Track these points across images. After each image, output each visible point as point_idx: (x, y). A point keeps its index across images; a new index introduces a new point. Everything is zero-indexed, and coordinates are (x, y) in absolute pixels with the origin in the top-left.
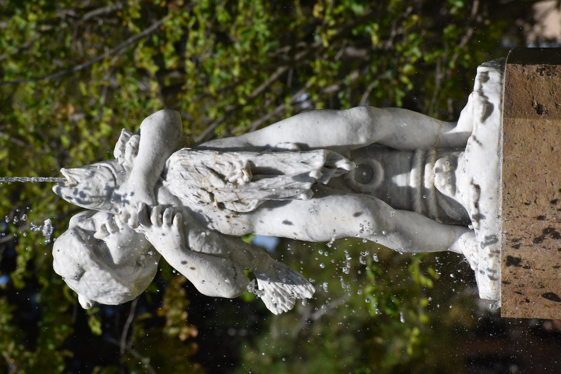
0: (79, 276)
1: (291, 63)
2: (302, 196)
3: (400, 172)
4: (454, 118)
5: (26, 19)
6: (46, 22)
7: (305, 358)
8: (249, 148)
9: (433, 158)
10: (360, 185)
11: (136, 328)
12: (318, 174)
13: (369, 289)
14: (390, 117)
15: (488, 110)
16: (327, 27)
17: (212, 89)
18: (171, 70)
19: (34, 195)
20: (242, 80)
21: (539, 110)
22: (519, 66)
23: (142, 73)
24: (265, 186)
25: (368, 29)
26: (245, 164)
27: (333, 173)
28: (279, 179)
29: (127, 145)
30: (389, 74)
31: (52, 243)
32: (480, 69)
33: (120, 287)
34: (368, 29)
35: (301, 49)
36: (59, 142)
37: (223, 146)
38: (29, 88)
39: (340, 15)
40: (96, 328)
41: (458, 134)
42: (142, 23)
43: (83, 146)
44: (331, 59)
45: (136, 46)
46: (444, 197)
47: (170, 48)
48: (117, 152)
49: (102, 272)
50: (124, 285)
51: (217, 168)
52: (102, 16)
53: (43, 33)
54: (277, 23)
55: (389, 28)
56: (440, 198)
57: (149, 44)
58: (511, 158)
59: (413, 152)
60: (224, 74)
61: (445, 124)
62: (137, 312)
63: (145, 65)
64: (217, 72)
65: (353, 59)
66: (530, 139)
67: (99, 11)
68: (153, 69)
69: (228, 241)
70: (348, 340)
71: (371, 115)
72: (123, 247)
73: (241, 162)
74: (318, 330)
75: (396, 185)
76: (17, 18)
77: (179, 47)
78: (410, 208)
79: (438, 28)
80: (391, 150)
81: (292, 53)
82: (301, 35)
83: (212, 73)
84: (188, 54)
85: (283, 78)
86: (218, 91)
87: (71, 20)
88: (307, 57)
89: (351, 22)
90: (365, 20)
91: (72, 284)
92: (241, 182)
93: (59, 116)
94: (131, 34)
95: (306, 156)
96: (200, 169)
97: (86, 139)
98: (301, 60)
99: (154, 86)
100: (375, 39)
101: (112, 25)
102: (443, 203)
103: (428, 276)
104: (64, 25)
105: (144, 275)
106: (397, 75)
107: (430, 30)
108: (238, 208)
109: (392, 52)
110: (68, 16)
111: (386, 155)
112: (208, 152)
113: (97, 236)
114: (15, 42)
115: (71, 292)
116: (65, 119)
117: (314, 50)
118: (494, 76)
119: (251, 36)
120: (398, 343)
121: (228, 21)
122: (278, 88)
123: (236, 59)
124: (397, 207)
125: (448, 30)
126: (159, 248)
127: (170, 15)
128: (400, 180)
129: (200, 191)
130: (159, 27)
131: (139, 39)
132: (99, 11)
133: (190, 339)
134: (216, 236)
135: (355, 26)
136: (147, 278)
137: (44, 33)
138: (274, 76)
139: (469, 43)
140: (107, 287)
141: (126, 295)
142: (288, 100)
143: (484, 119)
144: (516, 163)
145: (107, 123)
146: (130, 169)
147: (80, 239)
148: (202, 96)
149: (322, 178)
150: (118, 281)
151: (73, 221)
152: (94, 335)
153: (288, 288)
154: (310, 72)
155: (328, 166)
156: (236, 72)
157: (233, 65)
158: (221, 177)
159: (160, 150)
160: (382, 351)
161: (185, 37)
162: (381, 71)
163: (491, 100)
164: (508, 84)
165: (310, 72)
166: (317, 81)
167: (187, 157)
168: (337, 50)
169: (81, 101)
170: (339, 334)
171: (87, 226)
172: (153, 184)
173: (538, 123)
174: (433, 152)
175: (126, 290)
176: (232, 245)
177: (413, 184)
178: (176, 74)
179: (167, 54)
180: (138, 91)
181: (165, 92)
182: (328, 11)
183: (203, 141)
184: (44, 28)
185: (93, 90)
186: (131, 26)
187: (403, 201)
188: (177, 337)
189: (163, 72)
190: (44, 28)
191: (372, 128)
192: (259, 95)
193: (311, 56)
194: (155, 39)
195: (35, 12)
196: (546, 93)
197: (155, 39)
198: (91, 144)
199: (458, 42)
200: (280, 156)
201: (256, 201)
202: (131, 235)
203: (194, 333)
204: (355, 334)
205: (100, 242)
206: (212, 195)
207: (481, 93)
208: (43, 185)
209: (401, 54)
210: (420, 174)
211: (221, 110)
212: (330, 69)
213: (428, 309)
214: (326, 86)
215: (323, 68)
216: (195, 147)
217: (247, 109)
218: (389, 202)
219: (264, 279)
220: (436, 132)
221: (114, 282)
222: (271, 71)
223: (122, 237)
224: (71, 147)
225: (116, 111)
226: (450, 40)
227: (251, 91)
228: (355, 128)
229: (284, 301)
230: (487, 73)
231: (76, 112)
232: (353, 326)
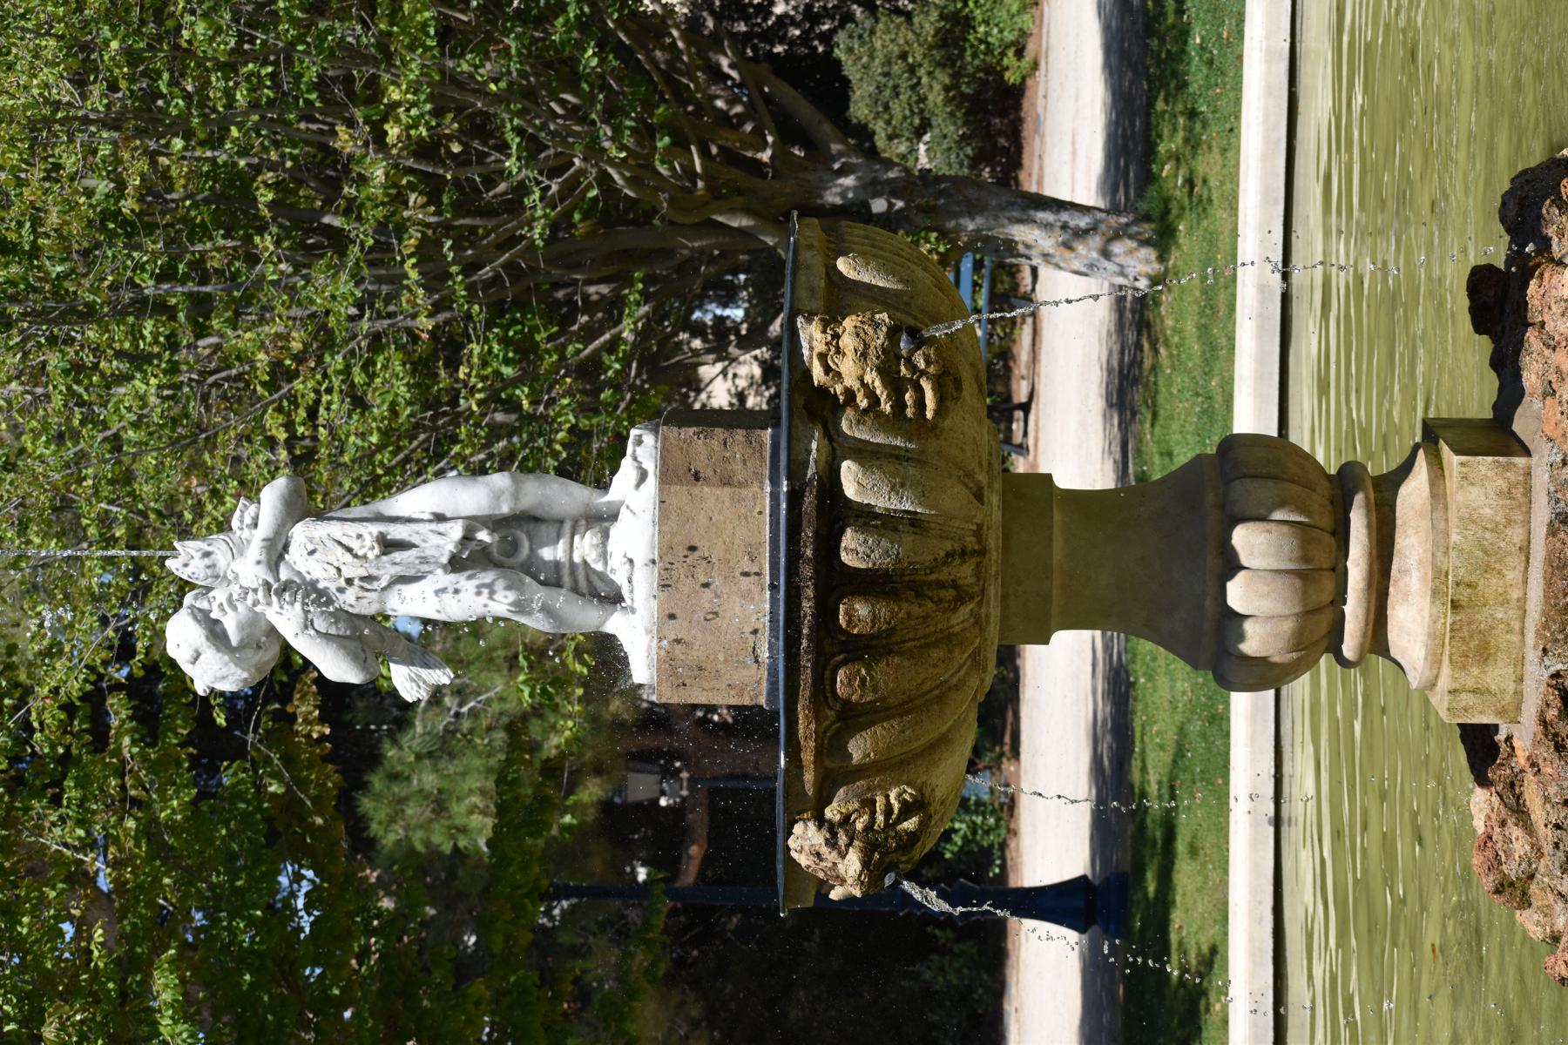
0: (196, 658)
1: (435, 428)
2: (439, 571)
3: (547, 545)
4: (603, 485)
6: (168, 387)
7: (452, 756)
8: (380, 518)
9: (582, 529)
10: (503, 559)
12: (456, 547)
14: (536, 484)
15: (643, 476)
18: (303, 437)
20: (380, 448)
21: (697, 477)
22: (675, 429)
24: (398, 560)
25: (518, 392)
27: (472, 546)
29: (246, 515)
32: (634, 432)
33: (239, 671)
34: (518, 392)
35: (445, 414)
38: (151, 460)
40: (221, 720)
41: (609, 503)
42: (271, 386)
45: (265, 412)
46: (595, 572)
47: (302, 413)
48: (235, 523)
49: (220, 655)
50: (243, 670)
51: (345, 541)
52: (227, 379)
53: (165, 399)
54: (417, 385)
56: (590, 573)
57: (279, 410)
58: (666, 528)
59: (561, 522)
60: (359, 442)
65: (503, 425)
66: (688, 508)
67: (224, 374)
69: (357, 622)
70: (500, 736)
71: (515, 481)
72: (241, 627)
73: (371, 534)
74: (466, 725)
75: (542, 559)
77: (312, 413)
78: (558, 584)
81: (434, 419)
82: (446, 399)
83: (347, 439)
84: (321, 421)
86: (353, 461)
87: (194, 384)
88: (450, 423)
90: (515, 382)
91: (187, 668)
92: (371, 555)
93: (182, 489)
94: (260, 399)
95: (442, 527)
96: (327, 541)
97: (209, 513)
98: (443, 426)
99: (283, 454)
102: (595, 579)
103: (584, 663)
104: (186, 389)
105: (266, 658)
106: (550, 443)
109: (544, 417)
110: (191, 380)
111: (531, 526)
112: (334, 522)
113: (213, 615)
116: (188, 493)
118: (649, 439)
119: (390, 398)
121: (365, 384)
125: (606, 395)
127: (301, 378)
128: (547, 554)
129: (326, 566)
130: (289, 390)
132: (224, 374)
134: (344, 616)
135: (504, 389)
136: (267, 662)
137: (167, 398)
139: (627, 408)
140: (224, 671)
143: (638, 486)
146: (249, 542)
147: (195, 618)
148: (337, 465)
149: (461, 552)
150: (236, 665)
151: (188, 599)
152: (219, 727)
153: (424, 673)
154: (454, 440)
155: (467, 538)
158: (349, 550)
159: (283, 520)
161: (317, 402)
162: (532, 438)
163: (644, 466)
164: (663, 448)
166: (463, 448)
167: (312, 528)
169: (206, 474)
170: (489, 729)
172: (274, 558)
173: (696, 491)
174: (583, 522)
175: (245, 675)
178: (307, 442)
181: (295, 461)
182: (474, 373)
184: (166, 392)
185: (219, 460)
190: (166, 392)
191: (516, 496)
192: (398, 464)
193: (456, 420)
194: (285, 403)
195: (156, 376)
197: (285, 403)
200: (414, 526)
201: (388, 577)
202: (251, 614)
203: (327, 731)
205: (217, 622)
206: (339, 570)
207: (635, 459)
209: (554, 420)
210: (568, 546)
212: (476, 435)
214: (472, 455)
216: (320, 516)
219: (396, 662)
220: (586, 501)
221: (232, 666)
222: (413, 438)
223: (241, 617)
226: (608, 404)
227: (390, 461)
228: (497, 496)
229: (419, 687)
230: (640, 436)
232: (505, 720)
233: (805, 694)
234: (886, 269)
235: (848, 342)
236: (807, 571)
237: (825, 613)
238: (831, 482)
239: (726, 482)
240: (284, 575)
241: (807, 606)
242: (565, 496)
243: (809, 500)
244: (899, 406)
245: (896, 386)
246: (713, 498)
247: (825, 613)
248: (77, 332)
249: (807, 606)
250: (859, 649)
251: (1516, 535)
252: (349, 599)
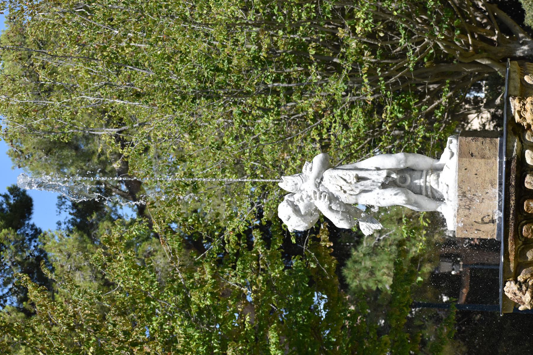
1: (373, 136)
2: (377, 188)
4: (438, 158)
5: (269, 119)
6: (277, 120)
8: (356, 169)
11: (309, 240)
13: (403, 227)
15: (452, 154)
16: (387, 123)
17: (341, 147)
18: (325, 139)
19: (270, 188)
20: (353, 143)
21: (472, 155)
22: (464, 138)
23: (314, 140)
26: (354, 175)
28: (368, 181)
30: (412, 141)
31: (277, 206)
32: (449, 139)
33: (304, 224)
34: (404, 123)
35: (377, 131)
36: (280, 167)
37: (346, 168)
39: (392, 118)
40: (294, 241)
43: (289, 169)
44: (389, 135)
45: (311, 130)
47: (325, 130)
51: (344, 177)
52: (298, 118)
53: (275, 124)
54: (367, 120)
55: (412, 123)
57: (317, 129)
59: (422, 171)
60: (346, 141)
61: (436, 160)
62: (310, 234)
63: (315, 137)
64: (343, 140)
68: (318, 139)
69: (347, 206)
70: (394, 247)
71: (406, 156)
74: (382, 243)
76: (265, 119)
77: (328, 130)
78: (421, 194)
79: (431, 123)
80: (413, 170)
81: (373, 133)
85: (369, 143)
86: (344, 148)
89: (396, 120)
90: (402, 120)
92: (353, 183)
93: (281, 158)
95: (380, 172)
96: (337, 177)
99: (318, 145)
100: (406, 128)
101: (301, 121)
103: (427, 222)
104: (283, 121)
106: (415, 142)
107: (427, 124)
108: (352, 193)
109: (413, 133)
110: (285, 118)
111: (411, 172)
114: (264, 128)
115: (285, 226)
116: (283, 159)
117: (383, 131)
118: (455, 141)
120: (414, 249)
122: (367, 146)
123: (351, 135)
124: (415, 193)
126: (320, 208)
131: (313, 127)
133: (330, 247)
135: (398, 122)
137: (275, 124)
138: (366, 142)
139: (443, 129)
140: (299, 224)
141: (306, 227)
142: (371, 151)
144: (463, 176)
145: (299, 160)
149: (386, 181)
151: (286, 197)
152: (294, 244)
154: (380, 140)
155: (388, 176)
156: (351, 140)
157: (350, 137)
158: (345, 180)
160: (407, 252)
161: (331, 126)
162: (408, 140)
164: (460, 145)
165: (380, 140)
166: (383, 144)
168: (391, 131)
171: (291, 199)
173: (472, 160)
174: (430, 171)
175: (307, 225)
176: (349, 207)
177: (422, 184)
178: (327, 141)
179: (323, 133)
180: (313, 148)
182: (388, 116)
183: (338, 166)
186: (310, 122)
187: (418, 190)
188: (325, 246)
189: (321, 140)
190: (275, 122)
191: (406, 162)
192: (360, 149)
193: (381, 133)
194: (319, 127)
196: (475, 148)
197: (319, 127)
198: (293, 168)
199: (439, 129)
203: (332, 245)
204: (397, 245)
205: (296, 206)
208: (274, 184)
209: (417, 134)
211: (344, 155)
212: (388, 139)
213: (426, 235)
214: (386, 146)
215: (385, 138)
216: (334, 168)
217: (355, 154)
218: (412, 191)
221: (302, 222)
224: (285, 170)
225: (303, 155)
226: (436, 128)
228: (399, 162)
231: (287, 156)
232: (396, 242)
236: (512, 190)
238: (521, 158)
239: (483, 157)
243: (513, 164)
247: (521, 181)
249: (512, 203)
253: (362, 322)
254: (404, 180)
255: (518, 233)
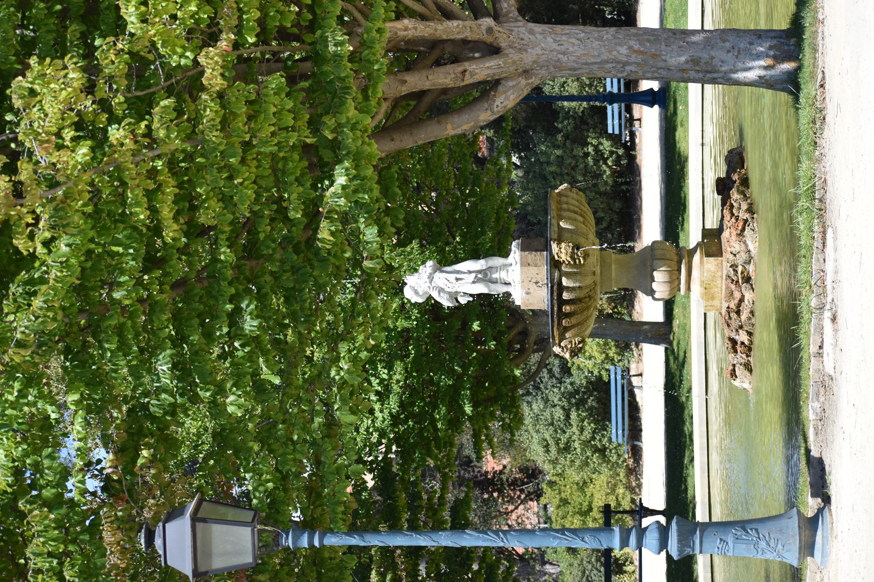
233: (555, 326)
234: (571, 224)
235: (563, 250)
236: (555, 302)
237: (560, 309)
238: (560, 283)
239: (536, 266)
240: (433, 284)
241: (556, 309)
242: (497, 261)
243: (555, 287)
244: (575, 262)
245: (574, 259)
246: (533, 270)
247: (560, 295)
248: (433, 422)
249: (556, 309)
250: (568, 315)
251: (719, 274)
252: (449, 290)
253: (182, 167)
254: (486, 275)
255: (559, 324)
